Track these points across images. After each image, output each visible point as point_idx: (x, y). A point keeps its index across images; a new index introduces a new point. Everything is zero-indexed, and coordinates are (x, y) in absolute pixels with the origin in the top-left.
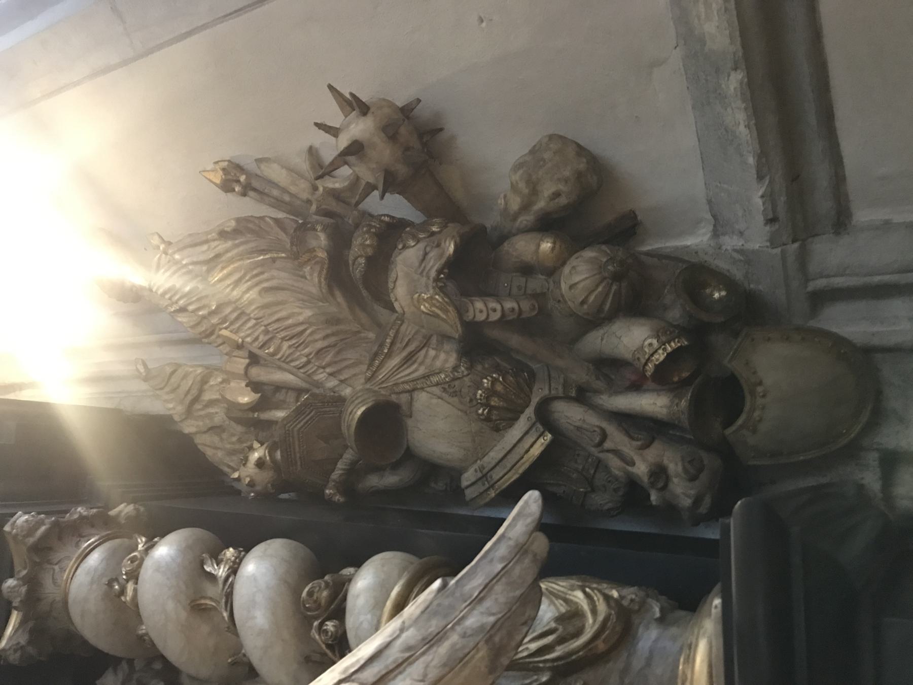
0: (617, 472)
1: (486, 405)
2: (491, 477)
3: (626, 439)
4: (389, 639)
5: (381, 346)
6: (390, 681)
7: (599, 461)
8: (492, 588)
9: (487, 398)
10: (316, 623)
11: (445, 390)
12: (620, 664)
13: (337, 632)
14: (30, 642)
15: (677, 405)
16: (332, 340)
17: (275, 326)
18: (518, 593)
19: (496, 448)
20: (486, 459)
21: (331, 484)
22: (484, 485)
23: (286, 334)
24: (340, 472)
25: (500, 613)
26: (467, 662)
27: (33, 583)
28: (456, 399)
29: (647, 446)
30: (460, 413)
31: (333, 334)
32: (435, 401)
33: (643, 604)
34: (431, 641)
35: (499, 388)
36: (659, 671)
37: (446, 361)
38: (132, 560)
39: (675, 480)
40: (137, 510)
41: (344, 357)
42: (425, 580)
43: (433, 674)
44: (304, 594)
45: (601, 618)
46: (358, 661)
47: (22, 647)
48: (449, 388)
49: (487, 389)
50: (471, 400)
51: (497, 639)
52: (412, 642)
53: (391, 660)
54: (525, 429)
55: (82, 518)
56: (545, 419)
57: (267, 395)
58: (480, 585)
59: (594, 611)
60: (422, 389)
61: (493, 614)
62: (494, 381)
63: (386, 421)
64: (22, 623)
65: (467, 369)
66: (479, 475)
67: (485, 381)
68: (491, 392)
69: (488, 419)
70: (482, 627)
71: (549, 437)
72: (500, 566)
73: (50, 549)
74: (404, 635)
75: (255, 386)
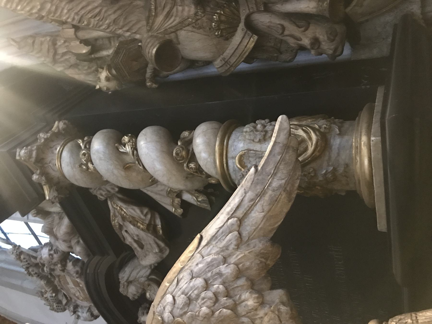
0: (293, 45)
1: (219, 29)
2: (230, 62)
3: (295, 28)
4: (241, 198)
5: (150, 10)
6: (249, 214)
7: (282, 40)
8: (278, 168)
9: (218, 26)
10: (185, 165)
11: (193, 27)
12: (326, 158)
13: (196, 167)
14: (59, 194)
15: (321, 6)
16: (119, 12)
17: (83, 12)
18: (291, 167)
19: (229, 48)
20: (225, 54)
21: (148, 80)
22: (227, 66)
23: (92, 14)
24: (150, 74)
25: (285, 178)
26: (280, 200)
27: (44, 173)
28: (201, 30)
29: (306, 30)
30: (206, 37)
31: (118, 9)
32: (190, 34)
33: (330, 127)
34: (260, 195)
35: (223, 18)
36: (343, 157)
37: (189, 11)
38: (84, 154)
39: (323, 43)
40: (64, 124)
41: (130, 20)
42: (226, 138)
43: (266, 208)
44: (174, 155)
45: (314, 142)
46: (232, 209)
47: (57, 197)
48: (196, 25)
49: (217, 21)
50: (210, 29)
51: (288, 189)
52: (252, 197)
53: (246, 206)
54: (242, 36)
55: (46, 140)
56: (251, 27)
57: (94, 46)
58: (273, 167)
59: (310, 138)
60: (181, 29)
61: (283, 179)
62: (220, 14)
63: (168, 51)
64: (50, 188)
65: (203, 13)
66: (223, 62)
67: (215, 17)
68: (220, 22)
69: (221, 36)
70: (280, 186)
71: (256, 37)
72: (279, 157)
73: (43, 159)
74: (247, 195)
75: (85, 42)
